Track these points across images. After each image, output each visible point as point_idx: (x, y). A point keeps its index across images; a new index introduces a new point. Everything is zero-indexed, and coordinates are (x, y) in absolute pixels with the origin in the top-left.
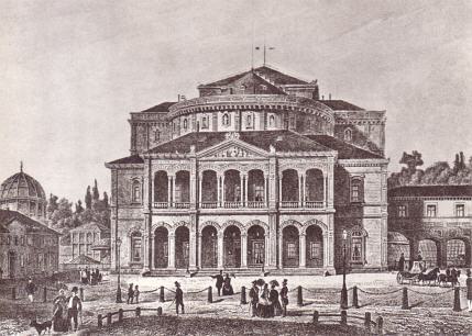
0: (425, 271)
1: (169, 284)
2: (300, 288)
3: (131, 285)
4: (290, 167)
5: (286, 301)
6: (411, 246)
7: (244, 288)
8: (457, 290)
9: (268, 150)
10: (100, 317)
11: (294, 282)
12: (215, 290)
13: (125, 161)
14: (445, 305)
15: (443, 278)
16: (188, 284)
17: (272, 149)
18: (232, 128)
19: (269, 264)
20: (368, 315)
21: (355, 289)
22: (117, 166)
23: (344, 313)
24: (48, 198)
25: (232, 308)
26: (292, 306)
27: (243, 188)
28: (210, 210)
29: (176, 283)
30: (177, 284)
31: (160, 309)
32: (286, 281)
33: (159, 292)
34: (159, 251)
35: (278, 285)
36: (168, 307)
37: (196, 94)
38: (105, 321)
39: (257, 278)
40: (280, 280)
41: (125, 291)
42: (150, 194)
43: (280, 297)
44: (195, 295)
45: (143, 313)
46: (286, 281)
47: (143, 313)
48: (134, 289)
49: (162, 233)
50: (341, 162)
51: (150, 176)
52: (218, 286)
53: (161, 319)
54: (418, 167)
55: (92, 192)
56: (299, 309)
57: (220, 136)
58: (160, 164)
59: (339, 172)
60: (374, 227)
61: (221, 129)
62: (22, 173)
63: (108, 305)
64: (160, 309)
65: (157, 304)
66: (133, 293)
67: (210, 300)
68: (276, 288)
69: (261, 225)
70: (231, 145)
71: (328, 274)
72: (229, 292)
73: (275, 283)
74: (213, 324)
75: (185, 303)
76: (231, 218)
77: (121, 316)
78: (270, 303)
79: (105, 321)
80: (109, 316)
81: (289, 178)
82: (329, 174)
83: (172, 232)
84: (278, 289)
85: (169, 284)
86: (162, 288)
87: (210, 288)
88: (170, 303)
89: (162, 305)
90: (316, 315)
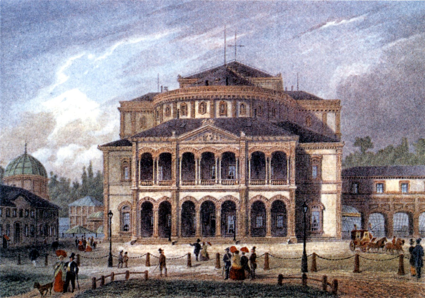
0: (374, 239)
1: (153, 250)
2: (267, 254)
3: (122, 252)
4: (188, 151)
5: (255, 266)
6: (362, 216)
7: (218, 255)
8: (402, 257)
9: (239, 135)
10: (94, 279)
11: (261, 250)
12: (193, 256)
13: (117, 144)
14: (392, 270)
15: (389, 248)
16: (169, 251)
17: (243, 134)
18: (207, 116)
19: (240, 230)
20: (325, 278)
21: (314, 255)
22: (109, 148)
23: (305, 277)
24: (49, 176)
25: (209, 270)
26: (259, 270)
27: (217, 168)
28: (148, 187)
29: (160, 250)
30: (160, 250)
31: (146, 272)
32: (254, 248)
33: (145, 257)
34: (156, 221)
35: (247, 251)
36: (153, 271)
37: (176, 86)
38: (98, 283)
39: (229, 246)
40: (250, 248)
41: (116, 255)
42: (137, 171)
43: (249, 262)
44: (175, 260)
45: (131, 276)
46: (254, 248)
47: (131, 276)
48: (123, 254)
49: (147, 206)
50: (303, 145)
51: (137, 157)
52: (197, 252)
53: (147, 284)
54: (369, 150)
55: (87, 172)
56: (267, 272)
57: (198, 123)
58: (145, 147)
59: (300, 155)
60: (329, 200)
61: (198, 116)
62: (26, 154)
63: (103, 270)
64: (146, 272)
65: (143, 268)
66: (124, 259)
67: (189, 264)
68: (246, 254)
69: (262, 200)
70: (207, 130)
71: (290, 242)
72: (206, 258)
73: (245, 250)
74: (193, 288)
75: (167, 267)
76: (227, 193)
77: (113, 278)
78: (242, 270)
79: (98, 283)
80: (103, 278)
81: (258, 160)
82: (291, 156)
83: (156, 208)
84: (248, 255)
85: (153, 250)
86: (148, 254)
87: (189, 255)
88: (154, 267)
89: (148, 268)
90: (281, 277)
